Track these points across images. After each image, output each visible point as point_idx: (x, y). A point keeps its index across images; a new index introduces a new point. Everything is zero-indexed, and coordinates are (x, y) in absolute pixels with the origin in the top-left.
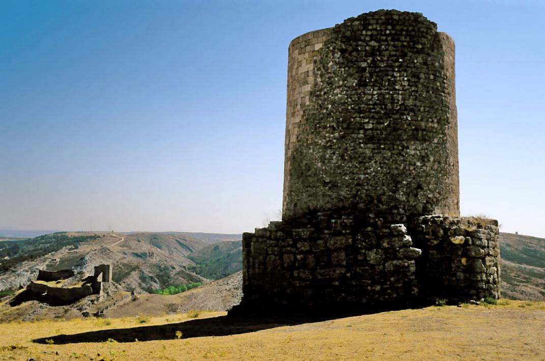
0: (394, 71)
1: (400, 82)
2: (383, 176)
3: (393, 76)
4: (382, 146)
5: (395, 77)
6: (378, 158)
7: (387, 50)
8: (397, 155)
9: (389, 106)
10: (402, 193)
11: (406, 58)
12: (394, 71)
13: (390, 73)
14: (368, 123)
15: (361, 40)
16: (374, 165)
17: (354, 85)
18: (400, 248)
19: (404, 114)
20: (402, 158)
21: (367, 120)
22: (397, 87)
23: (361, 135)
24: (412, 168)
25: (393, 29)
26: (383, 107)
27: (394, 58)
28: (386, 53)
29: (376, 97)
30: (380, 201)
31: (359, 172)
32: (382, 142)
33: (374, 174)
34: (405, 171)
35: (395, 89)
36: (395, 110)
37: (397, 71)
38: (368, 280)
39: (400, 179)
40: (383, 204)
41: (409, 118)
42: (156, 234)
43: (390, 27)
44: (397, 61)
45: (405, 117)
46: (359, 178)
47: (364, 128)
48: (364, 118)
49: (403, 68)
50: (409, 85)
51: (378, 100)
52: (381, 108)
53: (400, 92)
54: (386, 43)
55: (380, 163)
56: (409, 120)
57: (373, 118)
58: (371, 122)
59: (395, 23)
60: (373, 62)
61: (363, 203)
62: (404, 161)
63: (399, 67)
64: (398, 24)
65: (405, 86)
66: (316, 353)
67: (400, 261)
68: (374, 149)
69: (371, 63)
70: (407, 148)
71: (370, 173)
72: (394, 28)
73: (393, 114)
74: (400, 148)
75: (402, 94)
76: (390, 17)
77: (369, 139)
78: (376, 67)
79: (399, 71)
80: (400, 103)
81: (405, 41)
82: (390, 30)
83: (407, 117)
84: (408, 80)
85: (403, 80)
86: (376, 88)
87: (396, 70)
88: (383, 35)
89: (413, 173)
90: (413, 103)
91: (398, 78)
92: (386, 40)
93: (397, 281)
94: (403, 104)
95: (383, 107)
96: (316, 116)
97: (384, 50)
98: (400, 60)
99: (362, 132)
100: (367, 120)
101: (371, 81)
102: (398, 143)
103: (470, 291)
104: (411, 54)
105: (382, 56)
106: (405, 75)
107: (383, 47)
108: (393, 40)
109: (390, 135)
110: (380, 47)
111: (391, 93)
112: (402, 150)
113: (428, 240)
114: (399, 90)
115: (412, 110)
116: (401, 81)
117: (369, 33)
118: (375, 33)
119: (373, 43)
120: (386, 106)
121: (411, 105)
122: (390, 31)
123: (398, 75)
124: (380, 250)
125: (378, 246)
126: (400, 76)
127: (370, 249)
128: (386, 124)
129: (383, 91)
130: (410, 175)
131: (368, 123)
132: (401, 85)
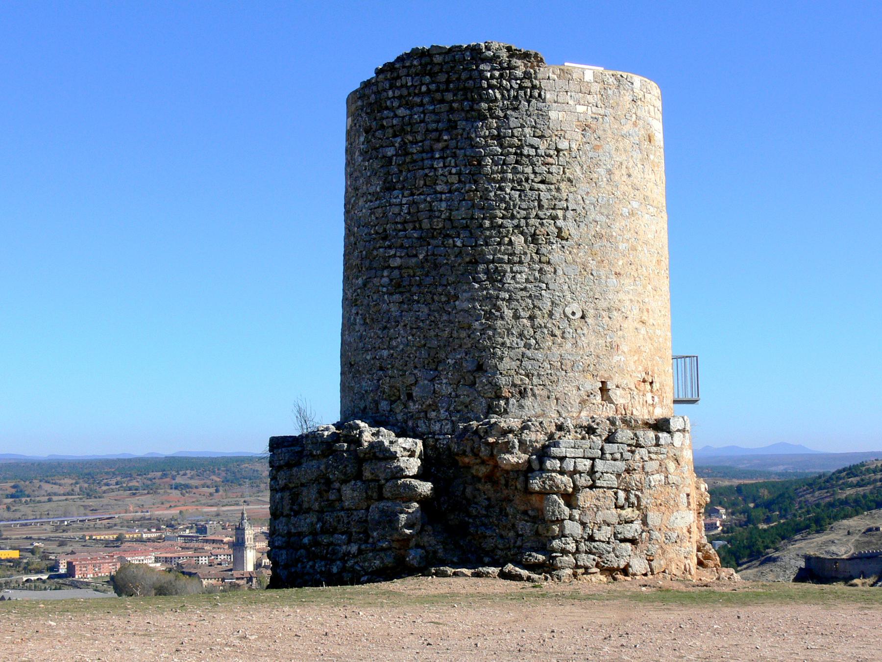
0: (433, 158)
1: (444, 179)
2: (416, 351)
3: (432, 167)
4: (416, 298)
5: (436, 169)
6: (408, 318)
7: (422, 121)
8: (438, 311)
9: (426, 224)
10: (444, 381)
11: (455, 132)
12: (433, 158)
13: (427, 163)
14: (395, 256)
15: (387, 108)
16: (402, 332)
17: (378, 190)
18: (387, 480)
19: (448, 236)
20: (445, 317)
21: (392, 252)
22: (438, 188)
23: (385, 280)
24: (463, 334)
25: (433, 82)
26: (417, 225)
27: (434, 135)
28: (422, 127)
29: (405, 209)
30: (410, 396)
31: (382, 347)
32: (414, 289)
33: (401, 347)
34: (451, 340)
35: (436, 192)
36: (435, 229)
37: (438, 159)
38: (343, 535)
39: (442, 355)
40: (414, 402)
41: (459, 244)
42: (174, 457)
43: (427, 79)
44: (438, 140)
45: (451, 241)
46: (381, 357)
47: (389, 267)
48: (390, 247)
49: (448, 152)
50: (460, 181)
51: (409, 213)
52: (414, 229)
53: (444, 196)
54: (421, 109)
55: (411, 328)
56: (458, 247)
57: (402, 246)
58: (398, 254)
59: (436, 69)
60: (404, 144)
61: (385, 399)
62: (450, 322)
63: (443, 150)
64: (441, 71)
65: (453, 183)
66: (238, 651)
67: (389, 504)
68: (402, 302)
69: (400, 147)
70: (457, 298)
71: (397, 347)
72: (433, 79)
73: (433, 237)
74: (444, 299)
75: (447, 200)
76: (427, 59)
77: (397, 286)
78: (407, 154)
79: (443, 158)
80: (443, 216)
81: (453, 101)
82: (427, 85)
83: (454, 241)
84: (459, 174)
85: (450, 173)
86: (406, 193)
87: (437, 156)
88: (415, 95)
89: (465, 344)
90: (467, 214)
91: (440, 172)
92: (422, 104)
93: (383, 538)
94: (449, 219)
95: (417, 225)
96: (536, 226)
97: (417, 123)
98: (445, 137)
99: (386, 273)
100: (392, 252)
101: (400, 180)
102: (440, 289)
103: (544, 561)
104: (464, 123)
105: (416, 132)
106: (453, 164)
107: (416, 117)
108: (432, 102)
109: (427, 276)
110: (411, 116)
111: (428, 199)
112: (448, 302)
113: (468, 467)
114: (441, 193)
115: (466, 227)
116: (446, 176)
117: (397, 93)
118: (405, 92)
119: (401, 112)
120: (420, 222)
121: (463, 219)
122: (428, 87)
123: (441, 165)
124: (359, 484)
125: (359, 476)
126: (445, 167)
127: (345, 482)
128: (421, 257)
129: (415, 197)
130: (460, 346)
131: (395, 256)
132: (447, 183)
